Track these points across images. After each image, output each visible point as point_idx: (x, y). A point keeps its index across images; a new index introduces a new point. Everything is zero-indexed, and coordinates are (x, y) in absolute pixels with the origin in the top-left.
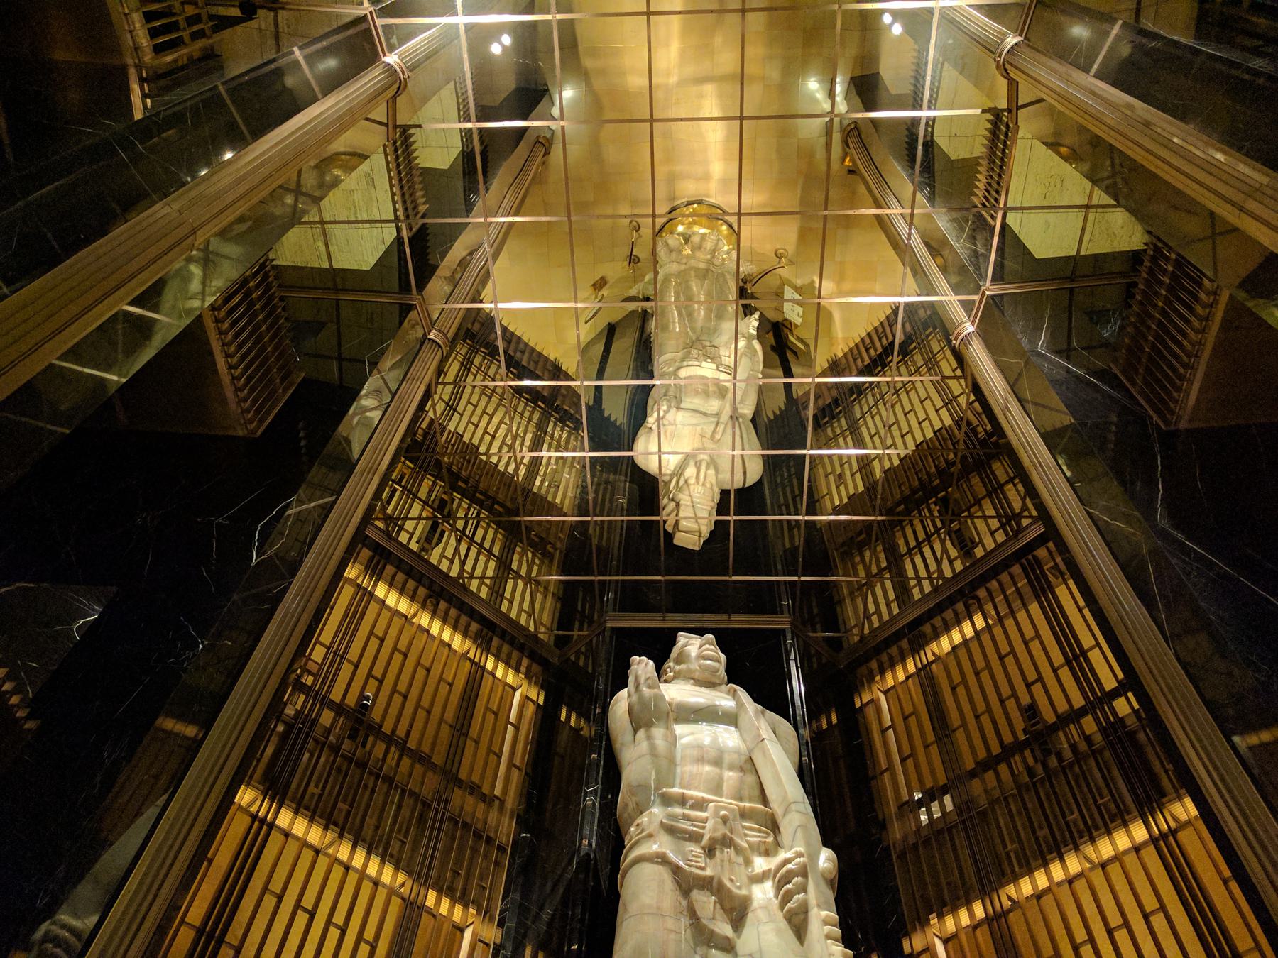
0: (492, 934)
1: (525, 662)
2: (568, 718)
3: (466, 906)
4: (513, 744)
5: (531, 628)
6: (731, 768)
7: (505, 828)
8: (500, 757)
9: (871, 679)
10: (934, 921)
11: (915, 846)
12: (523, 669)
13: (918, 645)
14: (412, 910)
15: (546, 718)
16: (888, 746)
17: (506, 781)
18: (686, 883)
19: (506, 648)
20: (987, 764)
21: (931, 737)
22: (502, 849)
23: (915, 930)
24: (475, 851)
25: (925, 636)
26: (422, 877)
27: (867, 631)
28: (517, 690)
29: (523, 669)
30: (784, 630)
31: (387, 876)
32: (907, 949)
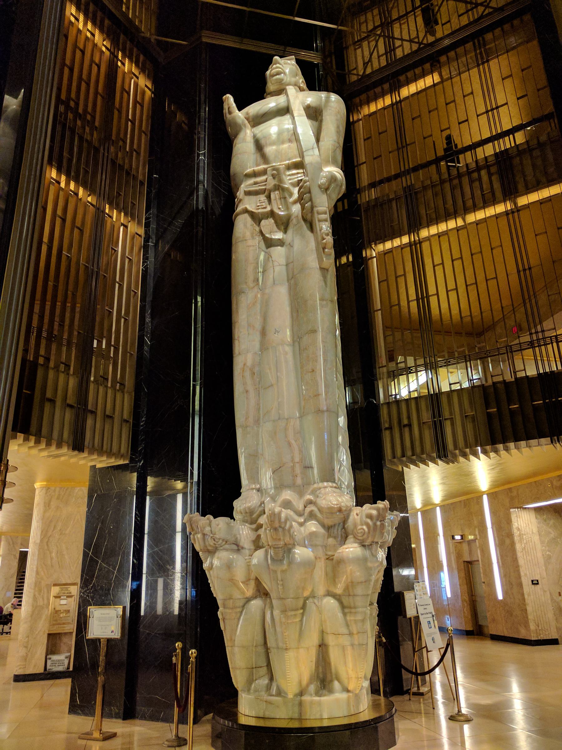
13: (396, 87)
18: (257, 218)
24: (127, 182)
25: (399, 81)
28: (137, 82)
31: (81, 191)
32: (364, 255)
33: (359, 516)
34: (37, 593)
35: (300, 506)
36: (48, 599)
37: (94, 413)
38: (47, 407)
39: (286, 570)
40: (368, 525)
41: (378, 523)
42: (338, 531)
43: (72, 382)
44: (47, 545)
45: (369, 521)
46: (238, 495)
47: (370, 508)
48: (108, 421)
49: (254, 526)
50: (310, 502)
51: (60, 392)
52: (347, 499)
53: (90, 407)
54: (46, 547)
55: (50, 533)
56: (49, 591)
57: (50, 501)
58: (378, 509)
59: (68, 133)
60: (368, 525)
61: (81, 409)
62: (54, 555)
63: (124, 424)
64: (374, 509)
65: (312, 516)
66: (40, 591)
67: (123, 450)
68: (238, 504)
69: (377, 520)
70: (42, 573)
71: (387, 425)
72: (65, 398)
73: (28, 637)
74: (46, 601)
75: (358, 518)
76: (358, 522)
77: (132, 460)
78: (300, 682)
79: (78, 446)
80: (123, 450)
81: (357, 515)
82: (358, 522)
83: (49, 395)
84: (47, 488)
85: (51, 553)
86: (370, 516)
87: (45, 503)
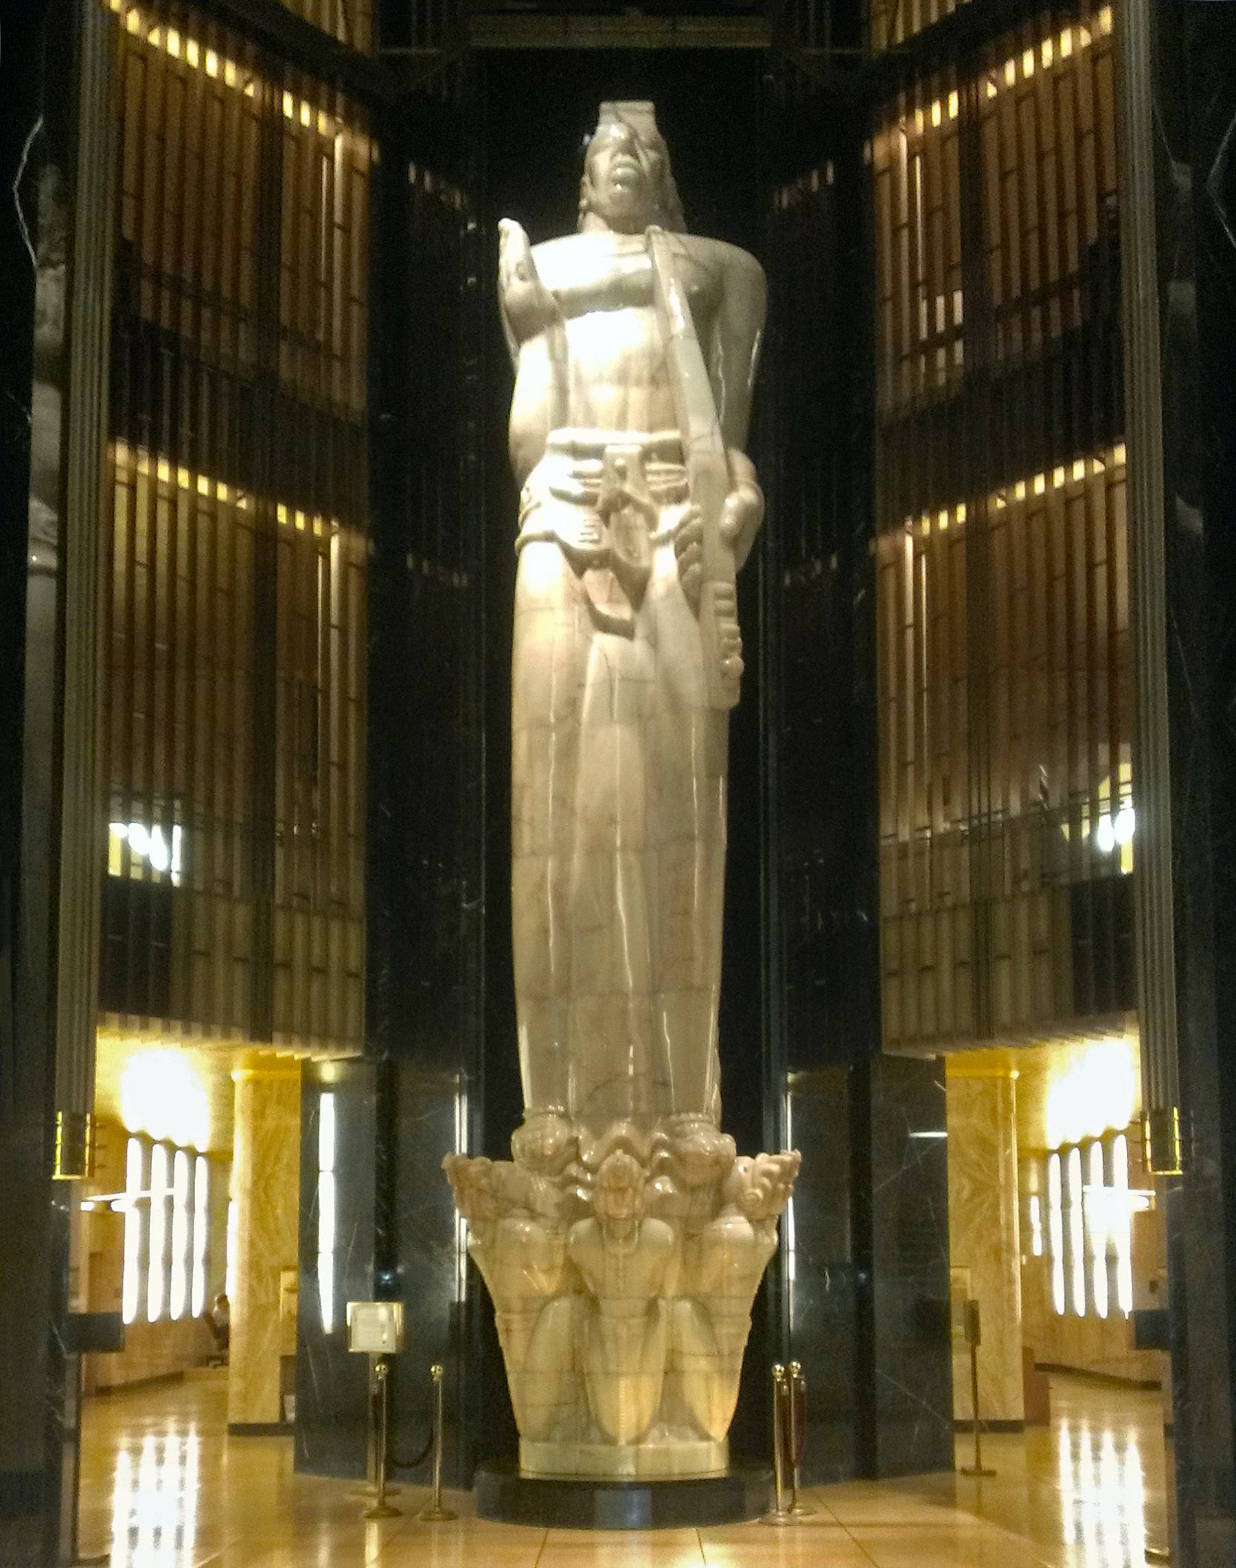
0: (360, 545)
1: (340, 99)
2: (420, 177)
3: (327, 521)
4: (341, 255)
5: (341, 36)
6: (638, 383)
7: (349, 391)
8: (329, 290)
9: (893, 120)
10: (909, 523)
11: (907, 420)
12: (339, 109)
14: (265, 535)
15: (384, 185)
16: (902, 251)
17: (344, 319)
18: (579, 563)
19: (306, 80)
20: (1028, 299)
21: (957, 258)
22: (383, 1326)
23: (885, 530)
26: (269, 489)
27: (900, 37)
28: (340, 144)
29: (339, 109)
30: (758, 52)
33: (750, 1173)
34: (255, 1283)
35: (645, 1151)
36: (277, 1294)
37: (288, 966)
38: (200, 965)
39: (632, 1255)
40: (763, 1188)
41: (781, 1186)
42: (706, 1197)
43: (242, 914)
44: (265, 1193)
45: (766, 1181)
46: (520, 1122)
47: (769, 1162)
48: (316, 961)
49: (557, 1179)
50: (659, 1145)
51: (220, 934)
52: (707, 1138)
53: (279, 956)
54: (263, 1198)
55: (269, 1170)
56: (277, 1280)
57: (265, 1107)
58: (782, 1164)
59: (187, 368)
60: (763, 1188)
61: (263, 962)
62: (279, 1211)
63: (352, 981)
64: (777, 1162)
65: (663, 1168)
66: (260, 1278)
67: (351, 1032)
68: (517, 1140)
69: (780, 1181)
70: (261, 1246)
71: (894, 965)
72: (229, 945)
73: (245, 1359)
74: (272, 1298)
75: (747, 1177)
76: (748, 1182)
77: (368, 1050)
78: (639, 1421)
79: (261, 1028)
80: (351, 1032)
81: (745, 1170)
82: (748, 1182)
83: (199, 945)
84: (256, 1083)
85: (274, 1208)
86: (768, 1174)
87: (253, 1111)
